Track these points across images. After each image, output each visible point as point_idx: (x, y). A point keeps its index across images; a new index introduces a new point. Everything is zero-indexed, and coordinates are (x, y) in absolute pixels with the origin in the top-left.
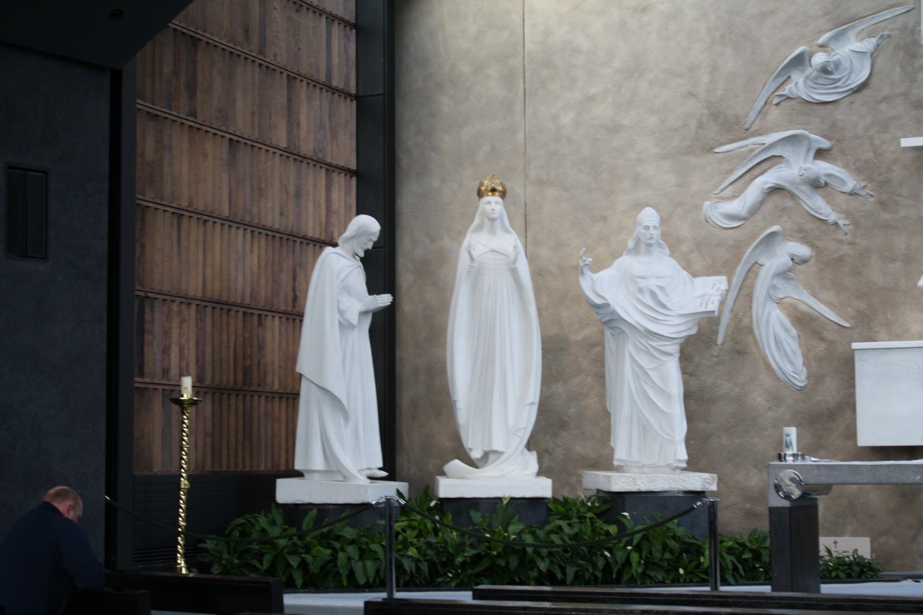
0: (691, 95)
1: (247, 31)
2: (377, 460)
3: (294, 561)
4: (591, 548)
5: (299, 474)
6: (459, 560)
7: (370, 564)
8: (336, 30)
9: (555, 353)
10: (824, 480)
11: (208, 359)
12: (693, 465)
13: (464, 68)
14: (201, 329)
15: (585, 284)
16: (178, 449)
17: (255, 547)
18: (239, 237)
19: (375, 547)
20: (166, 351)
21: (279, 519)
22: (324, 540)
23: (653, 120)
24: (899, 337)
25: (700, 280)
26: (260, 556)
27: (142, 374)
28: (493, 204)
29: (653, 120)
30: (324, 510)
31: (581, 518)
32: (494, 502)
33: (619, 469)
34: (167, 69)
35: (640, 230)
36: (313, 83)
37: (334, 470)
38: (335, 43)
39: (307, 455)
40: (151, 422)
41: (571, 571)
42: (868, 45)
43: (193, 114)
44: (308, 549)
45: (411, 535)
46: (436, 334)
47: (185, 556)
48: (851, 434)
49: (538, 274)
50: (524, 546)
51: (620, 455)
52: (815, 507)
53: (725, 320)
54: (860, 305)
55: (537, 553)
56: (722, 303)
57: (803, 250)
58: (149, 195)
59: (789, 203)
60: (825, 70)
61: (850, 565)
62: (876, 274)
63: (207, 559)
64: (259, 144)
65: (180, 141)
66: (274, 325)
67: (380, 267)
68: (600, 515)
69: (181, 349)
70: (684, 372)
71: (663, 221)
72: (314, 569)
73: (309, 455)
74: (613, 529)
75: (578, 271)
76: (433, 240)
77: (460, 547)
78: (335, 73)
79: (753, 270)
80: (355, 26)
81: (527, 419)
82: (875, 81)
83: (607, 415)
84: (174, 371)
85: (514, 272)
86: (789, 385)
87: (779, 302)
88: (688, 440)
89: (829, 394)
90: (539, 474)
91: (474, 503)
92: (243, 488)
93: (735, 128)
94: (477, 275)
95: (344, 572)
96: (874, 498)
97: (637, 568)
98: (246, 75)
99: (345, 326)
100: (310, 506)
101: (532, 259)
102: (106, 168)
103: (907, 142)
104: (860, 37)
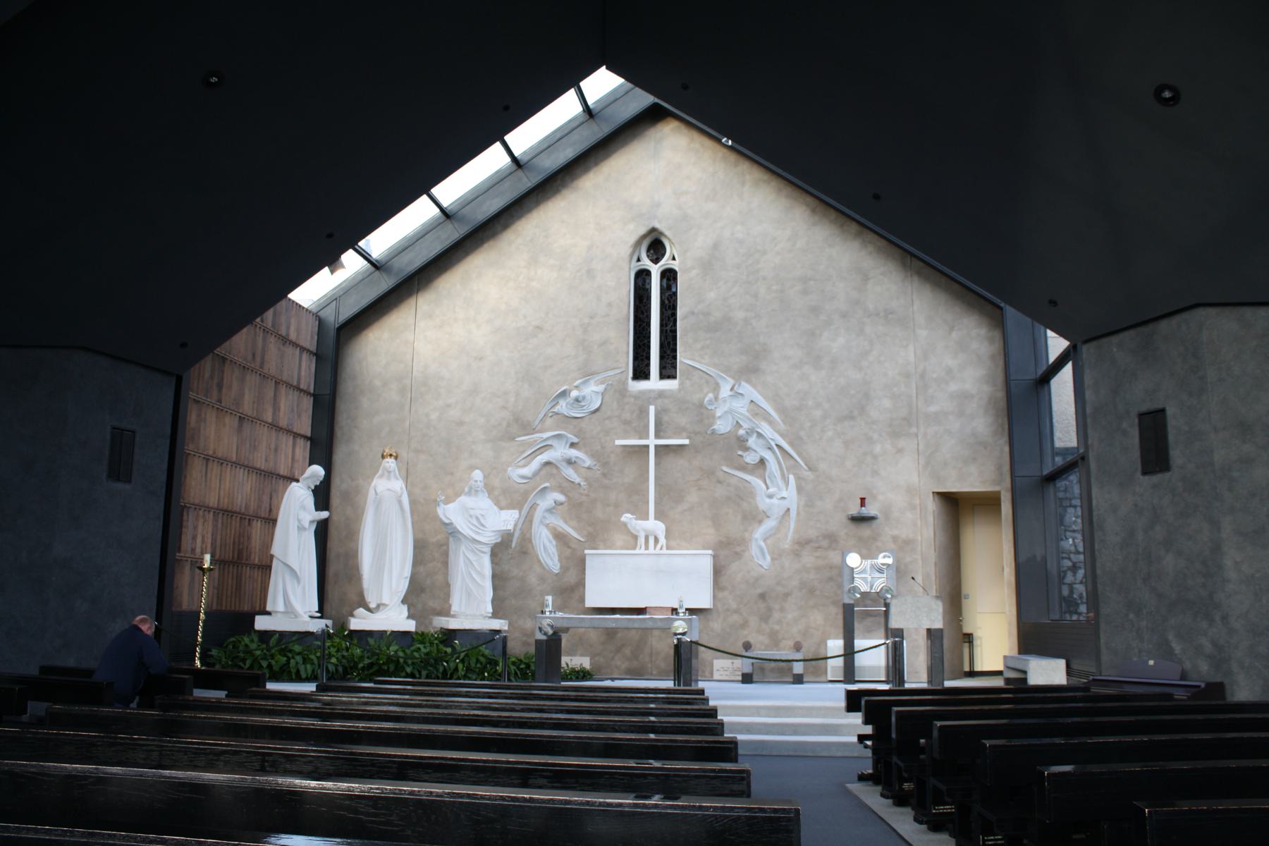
0: (504, 408)
1: (254, 355)
2: (315, 606)
3: (264, 664)
4: (436, 660)
5: (269, 613)
6: (361, 665)
7: (309, 666)
8: (305, 356)
9: (420, 548)
10: (565, 625)
11: (218, 543)
12: (495, 615)
13: (378, 383)
14: (215, 526)
15: (440, 511)
16: (198, 595)
17: (242, 655)
18: (241, 474)
19: (312, 657)
20: (194, 538)
21: (256, 639)
22: (283, 652)
23: (482, 420)
24: (610, 548)
25: (504, 512)
26: (244, 660)
27: (179, 551)
28: (390, 463)
29: (482, 420)
30: (283, 635)
31: (431, 644)
32: (382, 633)
33: (453, 616)
34: (207, 375)
35: (472, 482)
36: (289, 385)
37: (290, 611)
38: (304, 364)
39: (274, 602)
40: (184, 579)
41: (424, 673)
42: (601, 388)
43: (220, 401)
44: (272, 656)
45: (333, 650)
46: (352, 534)
47: (200, 659)
48: (582, 600)
49: (413, 502)
50: (399, 657)
51: (455, 608)
52: (560, 640)
53: (517, 534)
54: (590, 529)
55: (405, 662)
56: (515, 525)
57: (561, 498)
58: (191, 447)
59: (555, 471)
60: (577, 400)
61: (578, 672)
62: (600, 513)
63: (212, 661)
64: (256, 420)
65: (211, 416)
66: (257, 525)
67: (322, 496)
68: (442, 642)
69: (203, 537)
70: (493, 562)
71: (485, 477)
72: (276, 668)
73: (275, 601)
74: (449, 650)
75: (436, 503)
76: (353, 480)
77: (362, 658)
78: (303, 381)
79: (534, 507)
80: (316, 354)
81: (403, 586)
82: (603, 408)
83: (448, 585)
84: (198, 550)
85: (400, 502)
86: (550, 572)
87: (547, 526)
88: (493, 601)
89: (571, 578)
90: (409, 617)
91: (370, 633)
92: (235, 621)
93: (527, 428)
94: (378, 504)
95: (293, 671)
96: (593, 636)
97: (461, 672)
98: (252, 380)
99: (301, 528)
100: (274, 632)
101: (409, 495)
102: (169, 431)
103: (618, 442)
104: (597, 383)
